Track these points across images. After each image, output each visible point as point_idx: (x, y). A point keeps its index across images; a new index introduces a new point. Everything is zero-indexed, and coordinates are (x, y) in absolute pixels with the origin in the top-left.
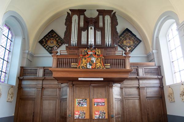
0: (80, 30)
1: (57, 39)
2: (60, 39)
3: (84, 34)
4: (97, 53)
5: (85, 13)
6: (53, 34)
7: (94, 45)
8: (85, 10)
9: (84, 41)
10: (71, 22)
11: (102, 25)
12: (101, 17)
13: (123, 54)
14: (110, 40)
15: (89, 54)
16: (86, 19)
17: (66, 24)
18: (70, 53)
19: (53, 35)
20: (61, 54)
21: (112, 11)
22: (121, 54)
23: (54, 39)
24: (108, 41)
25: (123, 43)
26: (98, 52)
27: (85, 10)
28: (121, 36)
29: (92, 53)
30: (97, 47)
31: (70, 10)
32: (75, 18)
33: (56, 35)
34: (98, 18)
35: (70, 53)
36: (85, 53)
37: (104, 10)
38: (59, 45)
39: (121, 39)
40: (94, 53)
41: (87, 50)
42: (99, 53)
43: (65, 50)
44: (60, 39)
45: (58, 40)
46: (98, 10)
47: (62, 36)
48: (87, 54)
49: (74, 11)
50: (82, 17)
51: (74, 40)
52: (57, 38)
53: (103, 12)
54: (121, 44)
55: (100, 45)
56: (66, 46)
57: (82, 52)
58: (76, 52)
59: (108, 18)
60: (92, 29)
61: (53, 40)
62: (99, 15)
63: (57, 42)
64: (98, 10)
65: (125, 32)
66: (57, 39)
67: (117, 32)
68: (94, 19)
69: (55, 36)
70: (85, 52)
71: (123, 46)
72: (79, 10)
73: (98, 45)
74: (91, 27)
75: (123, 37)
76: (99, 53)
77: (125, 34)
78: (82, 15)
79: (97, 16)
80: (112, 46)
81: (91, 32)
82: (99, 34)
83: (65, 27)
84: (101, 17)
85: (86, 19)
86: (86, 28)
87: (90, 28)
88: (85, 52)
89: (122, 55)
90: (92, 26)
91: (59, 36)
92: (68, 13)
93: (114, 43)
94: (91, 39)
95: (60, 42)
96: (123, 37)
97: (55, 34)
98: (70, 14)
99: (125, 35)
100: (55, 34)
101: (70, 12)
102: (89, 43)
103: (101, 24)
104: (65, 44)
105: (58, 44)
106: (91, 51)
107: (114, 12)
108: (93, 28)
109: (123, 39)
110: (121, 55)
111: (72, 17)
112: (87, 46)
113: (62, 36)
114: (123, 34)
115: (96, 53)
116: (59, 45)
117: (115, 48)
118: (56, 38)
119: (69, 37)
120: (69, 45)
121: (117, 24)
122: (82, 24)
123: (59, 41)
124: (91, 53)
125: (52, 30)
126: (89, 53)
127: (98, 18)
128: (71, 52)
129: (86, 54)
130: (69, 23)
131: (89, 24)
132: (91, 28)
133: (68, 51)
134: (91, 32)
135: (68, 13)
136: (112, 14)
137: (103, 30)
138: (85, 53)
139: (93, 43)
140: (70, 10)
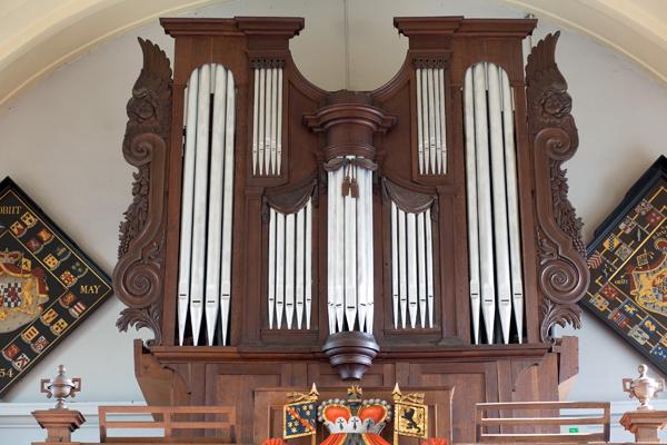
0: (257, 200)
1: (52, 263)
2: (73, 260)
3: (287, 233)
4: (401, 425)
5: (295, 44)
6: (16, 218)
7: (376, 338)
8: (296, 26)
9: (287, 300)
10: (173, 130)
11: (443, 157)
12: (430, 83)
13: (607, 427)
14: (511, 282)
15: (338, 436)
16: (300, 98)
17: (130, 150)
18: (182, 425)
19: (16, 228)
20: (111, 433)
21: (527, 26)
22: (600, 429)
23: (27, 264)
24: (498, 287)
25: (627, 288)
26: (409, 416)
27: (296, 26)
28: (607, 225)
29: (361, 428)
30: (404, 351)
31: (170, 25)
32: (210, 87)
33: (38, 227)
34: (405, 87)
35: (182, 425)
36: (301, 429)
37: (458, 23)
38: (69, 319)
39: (610, 255)
40: (376, 429)
41: (317, 404)
42: (412, 425)
43: (145, 403)
44: (73, 260)
45: (59, 271)
46: (399, 23)
47: (106, 249)
48: (322, 430)
49: (197, 37)
50: (269, 83)
51: (203, 290)
52: (51, 249)
53: (440, 44)
54: (613, 304)
55: (428, 332)
56: (137, 342)
57: (274, 413)
58: (232, 421)
59: (490, 91)
60: (356, 195)
61: (15, 267)
62: (414, 62)
63: (53, 288)
64: (399, 23)
65: (647, 195)
66: (52, 263)
67: (568, 211)
68: (374, 99)
69: (33, 233)
70: (302, 414)
71: (633, 320)
72: (239, 23)
73: (409, 334)
74: (351, 172)
75: (625, 239)
76: (412, 425)
77: (644, 207)
78: (268, 63)
79: (401, 73)
80: (532, 338)
81: (350, 214)
82: (414, 230)
83: (127, 173)
84: (430, 83)
85: (300, 98)
86: (301, 184)
87: (335, 181)
88: (302, 414)
89: (606, 436)
90: (357, 164)
91: (63, 240)
92: (150, 50)
93: (542, 313)
94: (351, 286)
95: (75, 289)
96: (633, 235)
97: (30, 220)
98: (170, 55)
99: (642, 220)
100: (30, 220)
101: (167, 45)
102: (334, 315)
103: (432, 149)
104: (132, 329)
105: (57, 308)
106: (355, 408)
107: (538, 36)
108: (365, 180)
109: (627, 253)
110: (594, 437)
111: (185, 85)
112: (317, 354)
113: (106, 249)
114: (632, 212)
115: (390, 425)
116: (69, 319)
117: (559, 359)
118: (42, 256)
119: (164, 266)
120: (159, 329)
121: (570, 143)
122: (269, 149)
123: (69, 281)
124: (348, 428)
125: (8, 181)
126: (334, 428)
127: (405, 87)
128: (213, 417)
129: (311, 431)
130: (159, 139)
131: (333, 149)
132: (350, 188)
133: (167, 411)
134: (350, 214)
135: (150, 50)
136: (526, 52)
137: (445, 199)
138: (301, 429)
139: (368, 314)
140: (170, 25)
